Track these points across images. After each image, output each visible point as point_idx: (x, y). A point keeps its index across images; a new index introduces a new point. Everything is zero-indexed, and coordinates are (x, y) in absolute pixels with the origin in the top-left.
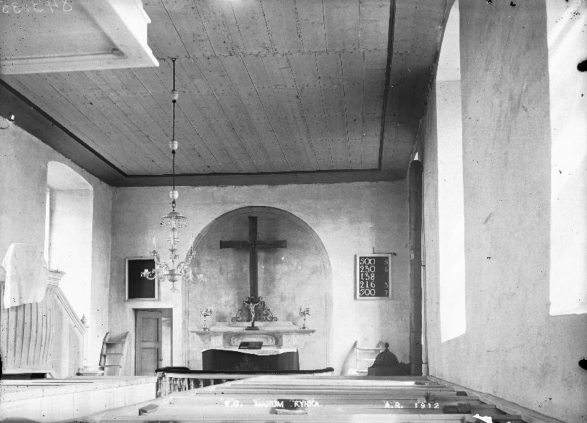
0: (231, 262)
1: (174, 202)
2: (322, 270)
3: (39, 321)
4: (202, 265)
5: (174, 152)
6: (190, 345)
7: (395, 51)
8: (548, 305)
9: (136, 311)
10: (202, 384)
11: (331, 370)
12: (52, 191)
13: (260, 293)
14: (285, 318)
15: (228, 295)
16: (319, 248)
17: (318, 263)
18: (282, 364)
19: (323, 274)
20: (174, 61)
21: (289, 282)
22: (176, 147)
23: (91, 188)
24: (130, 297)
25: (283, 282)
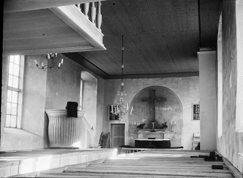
0: (144, 106)
1: (122, 87)
2: (180, 110)
3: (62, 131)
4: (136, 108)
5: (122, 69)
6: (131, 137)
7: (202, 30)
8: (235, 128)
9: (112, 124)
10: (134, 151)
11: (182, 147)
12: (84, 81)
13: (156, 118)
14: (95, 142)
15: (145, 119)
16: (178, 103)
17: (178, 107)
18: (164, 145)
19: (180, 111)
20: (123, 37)
21: (165, 113)
22: (123, 67)
23: (96, 80)
24: (110, 119)
25: (165, 114)
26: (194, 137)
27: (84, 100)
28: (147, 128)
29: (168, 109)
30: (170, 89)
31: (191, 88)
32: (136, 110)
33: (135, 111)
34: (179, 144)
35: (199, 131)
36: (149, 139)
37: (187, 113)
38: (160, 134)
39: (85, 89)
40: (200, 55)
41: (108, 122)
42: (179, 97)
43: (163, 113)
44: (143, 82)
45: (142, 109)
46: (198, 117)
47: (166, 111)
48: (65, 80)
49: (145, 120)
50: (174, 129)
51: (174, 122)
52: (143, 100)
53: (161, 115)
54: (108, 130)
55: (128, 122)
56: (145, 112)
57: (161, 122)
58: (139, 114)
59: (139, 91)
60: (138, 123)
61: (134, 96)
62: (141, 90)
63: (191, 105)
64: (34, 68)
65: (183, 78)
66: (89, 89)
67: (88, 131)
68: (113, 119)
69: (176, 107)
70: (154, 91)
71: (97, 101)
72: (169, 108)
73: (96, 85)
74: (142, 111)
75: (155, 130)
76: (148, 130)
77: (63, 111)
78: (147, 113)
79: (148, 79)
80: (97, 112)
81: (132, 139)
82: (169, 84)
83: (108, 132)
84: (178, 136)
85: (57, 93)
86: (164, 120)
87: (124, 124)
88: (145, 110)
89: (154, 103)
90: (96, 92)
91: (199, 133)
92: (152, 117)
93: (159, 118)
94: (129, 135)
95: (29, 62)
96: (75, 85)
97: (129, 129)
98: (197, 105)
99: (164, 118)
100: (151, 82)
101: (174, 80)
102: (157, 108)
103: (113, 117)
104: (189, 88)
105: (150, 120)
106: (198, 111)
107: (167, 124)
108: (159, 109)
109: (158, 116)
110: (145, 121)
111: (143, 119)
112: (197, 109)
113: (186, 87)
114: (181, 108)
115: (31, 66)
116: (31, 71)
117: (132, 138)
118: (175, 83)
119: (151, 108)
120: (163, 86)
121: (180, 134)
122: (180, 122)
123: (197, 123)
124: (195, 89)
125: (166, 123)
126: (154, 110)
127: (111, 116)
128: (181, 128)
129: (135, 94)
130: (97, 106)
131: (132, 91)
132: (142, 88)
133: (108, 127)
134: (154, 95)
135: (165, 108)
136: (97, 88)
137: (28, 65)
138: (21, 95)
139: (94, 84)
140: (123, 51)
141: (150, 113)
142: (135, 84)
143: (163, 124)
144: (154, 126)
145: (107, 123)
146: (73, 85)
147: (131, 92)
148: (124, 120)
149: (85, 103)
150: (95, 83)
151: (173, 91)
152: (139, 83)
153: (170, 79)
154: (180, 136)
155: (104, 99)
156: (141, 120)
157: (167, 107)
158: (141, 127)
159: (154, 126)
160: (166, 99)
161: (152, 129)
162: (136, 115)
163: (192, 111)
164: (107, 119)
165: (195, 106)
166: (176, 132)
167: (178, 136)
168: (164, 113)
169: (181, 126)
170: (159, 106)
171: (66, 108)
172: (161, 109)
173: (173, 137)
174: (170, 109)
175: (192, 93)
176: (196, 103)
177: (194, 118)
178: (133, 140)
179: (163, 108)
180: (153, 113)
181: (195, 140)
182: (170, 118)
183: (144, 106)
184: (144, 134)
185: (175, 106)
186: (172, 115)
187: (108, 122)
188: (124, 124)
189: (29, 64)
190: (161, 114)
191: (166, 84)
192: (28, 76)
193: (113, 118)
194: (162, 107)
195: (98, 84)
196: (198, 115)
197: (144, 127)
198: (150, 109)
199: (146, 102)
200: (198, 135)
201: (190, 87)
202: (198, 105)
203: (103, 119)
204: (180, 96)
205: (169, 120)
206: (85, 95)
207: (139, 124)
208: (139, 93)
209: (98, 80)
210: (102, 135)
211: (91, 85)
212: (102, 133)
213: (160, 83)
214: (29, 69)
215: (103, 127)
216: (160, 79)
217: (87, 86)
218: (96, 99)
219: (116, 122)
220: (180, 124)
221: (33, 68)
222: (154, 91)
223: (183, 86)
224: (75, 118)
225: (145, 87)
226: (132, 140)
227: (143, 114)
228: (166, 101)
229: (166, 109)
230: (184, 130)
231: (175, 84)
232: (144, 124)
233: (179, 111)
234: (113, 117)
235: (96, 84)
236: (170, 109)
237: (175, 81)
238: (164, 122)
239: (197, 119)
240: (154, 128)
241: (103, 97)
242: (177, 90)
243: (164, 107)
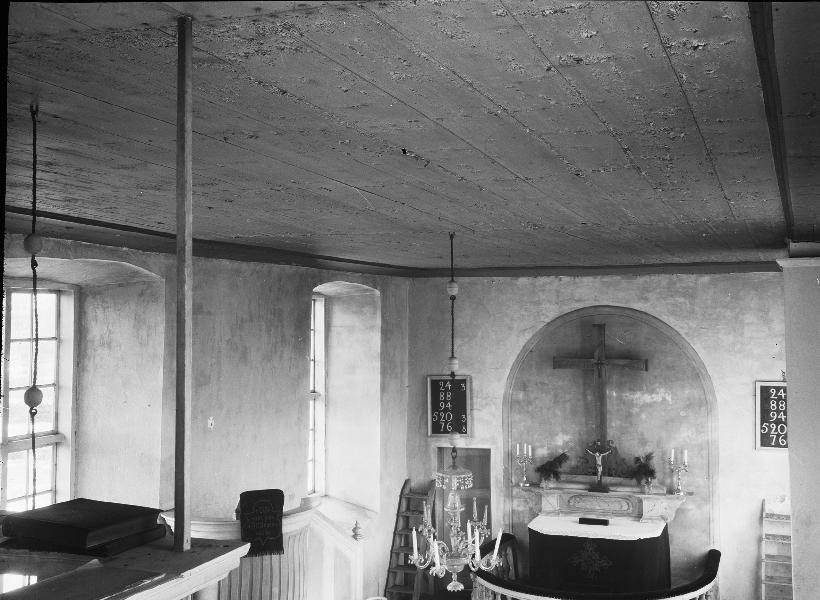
0: (564, 382)
2: (703, 404)
16: (696, 374)
19: (703, 409)
21: (647, 416)
23: (377, 292)
25: (643, 416)
26: (762, 516)
27: (333, 369)
28: (574, 471)
29: (657, 398)
30: (664, 318)
31: (749, 318)
32: (532, 396)
33: (529, 403)
34: (705, 538)
35: (788, 493)
36: (583, 521)
37: (734, 417)
38: (627, 499)
39: (334, 331)
40: (788, 269)
41: (426, 442)
42: (702, 353)
43: (638, 414)
44: (558, 292)
45: (556, 396)
46: (778, 436)
47: (650, 405)
48: (244, 356)
49: (567, 438)
50: (681, 481)
51: (680, 452)
52: (560, 361)
53: (631, 424)
54: (428, 472)
55: (500, 444)
56: (568, 405)
57: (632, 448)
58: (545, 411)
59: (540, 326)
60: (542, 447)
61: (523, 341)
62: (548, 320)
63: (751, 387)
64: (113, 344)
65: (717, 276)
66: (351, 329)
67: (338, 553)
68: (446, 432)
69: (689, 392)
70: (601, 327)
71: (384, 372)
72: (661, 395)
73: (375, 314)
74: (556, 402)
75: (608, 480)
76: (580, 478)
77: (229, 529)
78: (574, 413)
79: (577, 280)
80: (384, 412)
81: (521, 509)
82: (658, 299)
83: (427, 480)
84: (699, 507)
85: (211, 421)
86: (643, 442)
87: (489, 450)
88: (567, 397)
89: (600, 376)
90: (376, 338)
91: (788, 501)
92: (594, 426)
93: (623, 431)
94: (510, 496)
95: (93, 323)
96: (288, 352)
97: (506, 470)
98: (774, 387)
99: (642, 434)
100: (588, 292)
101: (678, 285)
102: (612, 393)
103: (446, 423)
104: (741, 317)
105: (585, 437)
106: (778, 412)
107: (655, 463)
108: (619, 399)
109: (618, 423)
110: (566, 443)
111: (560, 435)
112: (778, 405)
113: (728, 313)
114: (710, 398)
115: (102, 337)
116: (101, 360)
117: (518, 506)
118: (684, 296)
119: (589, 392)
120: (636, 306)
121: (707, 499)
122: (705, 452)
123: (777, 457)
124: (767, 321)
125: (649, 457)
126: (601, 398)
127: (440, 417)
128: (708, 478)
129: (528, 336)
130: (384, 388)
131: (515, 326)
132: (551, 312)
133: (430, 460)
134: (602, 344)
135: (643, 394)
136: (378, 322)
137: (90, 337)
138: (65, 455)
139: (366, 309)
140: (453, 298)
141: (587, 411)
142: (526, 298)
143: (637, 459)
144: (600, 469)
145: (423, 443)
146: (281, 357)
147: (510, 328)
148: (488, 428)
149: (334, 381)
150: (373, 303)
151: (676, 328)
152: (541, 294)
153: (663, 279)
154: (706, 508)
155: (410, 355)
156: (552, 435)
157: (652, 392)
158: (550, 469)
159: (600, 469)
160: (646, 361)
161: (595, 474)
162: (533, 417)
163: (752, 410)
164: (423, 431)
165: (765, 391)
166: (691, 490)
167: (699, 507)
168: (641, 411)
169: (710, 469)
170: (620, 386)
171: (237, 511)
172: (628, 395)
173: (680, 512)
174: (664, 399)
175: (751, 338)
176: (774, 375)
177: (765, 441)
178: (522, 512)
179: (638, 395)
180: (598, 412)
181: (769, 528)
182: (664, 434)
183: (560, 383)
184: (566, 497)
185: (683, 387)
186: (671, 422)
187: (429, 439)
188: (489, 450)
189: (95, 331)
190: (629, 415)
191: (646, 300)
192: (89, 378)
193: (445, 425)
194: (632, 390)
195: (384, 307)
196: (782, 429)
197: (565, 467)
198: (585, 396)
199: (569, 372)
200: (784, 508)
201: (743, 314)
202: (778, 389)
203: (409, 423)
204: (705, 348)
205: (659, 443)
206: (335, 351)
207: (543, 452)
208: (541, 332)
209: (383, 292)
210: (407, 491)
211: (359, 313)
212: (407, 482)
213: (621, 295)
214: (95, 350)
215: (408, 461)
216: (623, 278)
217: (341, 317)
218: (377, 364)
219: (460, 441)
220: (705, 462)
221: (109, 344)
222: (601, 327)
223: (715, 308)
224: (275, 557)
225: (566, 309)
226: (519, 513)
227: (559, 413)
228: (647, 370)
229: (647, 398)
230: (724, 484)
231: (682, 300)
232: (562, 458)
233: (700, 407)
234: (446, 423)
235: (375, 307)
236: (664, 399)
237: (685, 288)
238: (641, 452)
239: (777, 445)
240: (603, 474)
241: (406, 341)
242: (693, 324)
243: (641, 389)
